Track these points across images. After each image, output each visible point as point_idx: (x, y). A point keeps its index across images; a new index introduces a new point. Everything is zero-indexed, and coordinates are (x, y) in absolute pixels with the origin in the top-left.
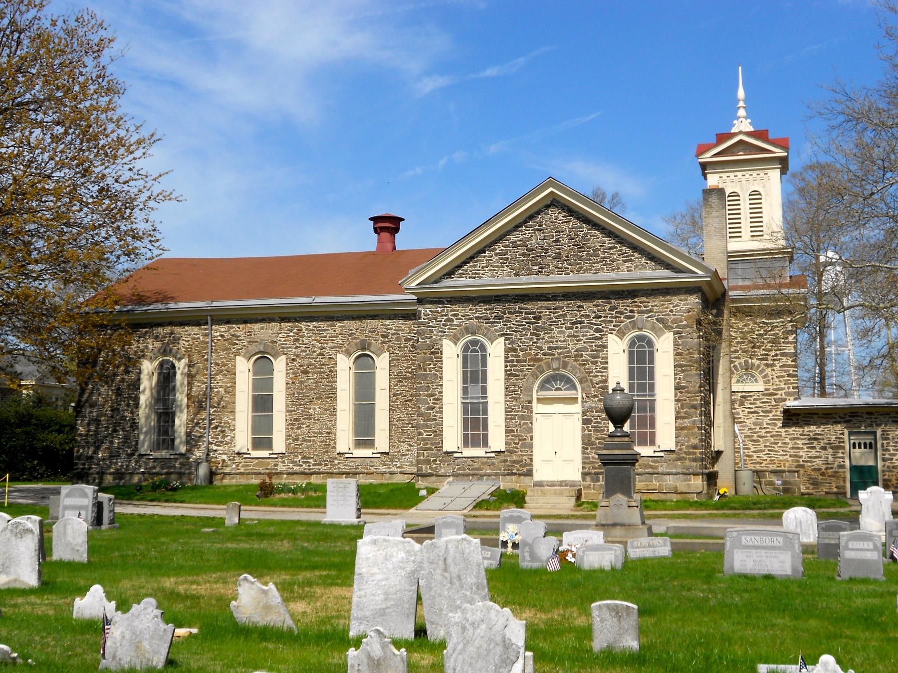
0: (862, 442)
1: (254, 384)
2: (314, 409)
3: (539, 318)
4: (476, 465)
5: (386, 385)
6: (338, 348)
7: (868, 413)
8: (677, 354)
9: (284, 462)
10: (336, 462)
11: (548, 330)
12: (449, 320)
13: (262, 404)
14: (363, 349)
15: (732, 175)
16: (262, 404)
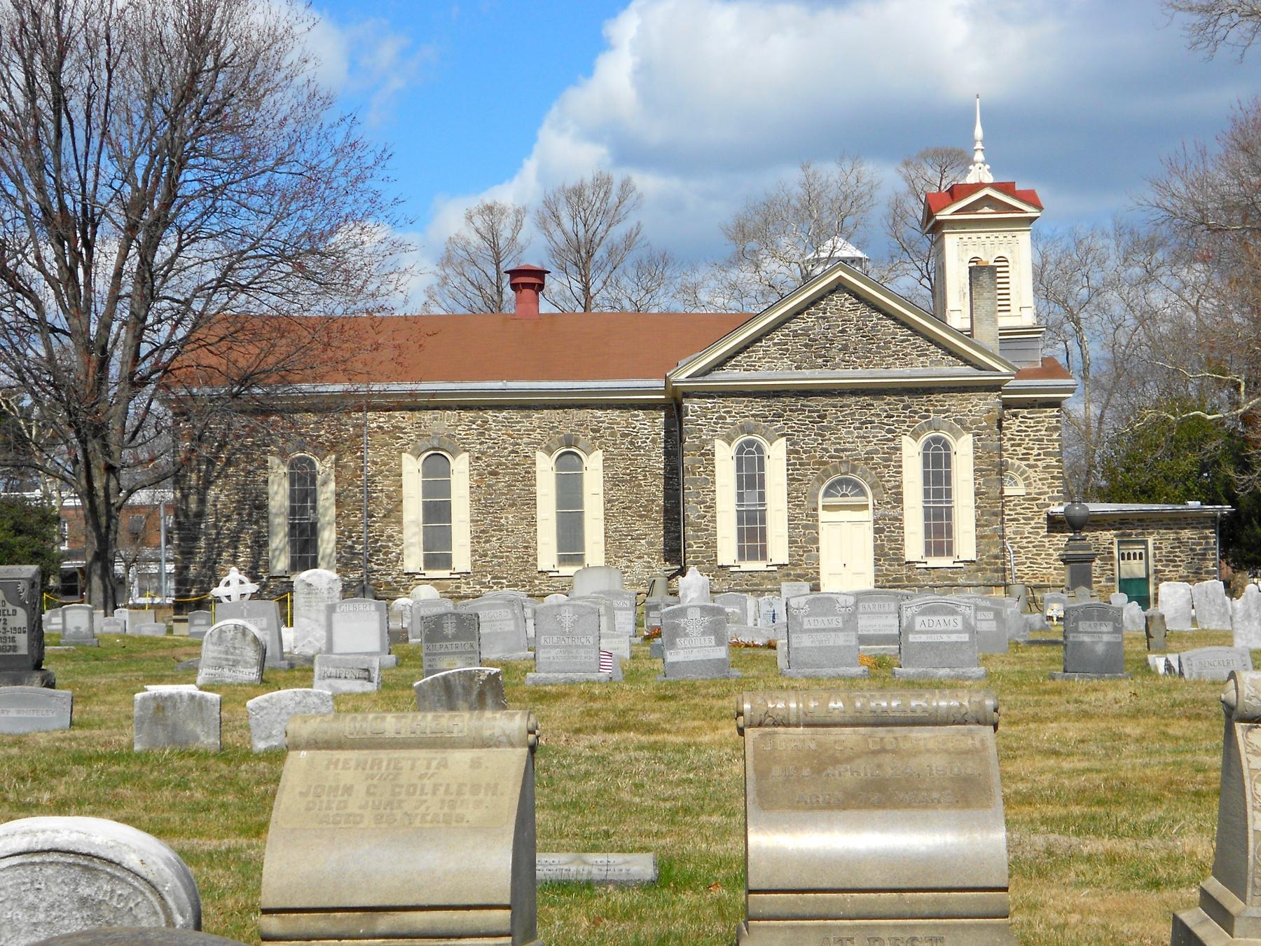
0: (1132, 552)
1: (424, 487)
2: (507, 518)
3: (824, 417)
4: (756, 581)
5: (600, 489)
6: (536, 444)
7: (1139, 520)
8: (976, 458)
9: (468, 583)
10: (537, 582)
11: (834, 430)
12: (721, 418)
13: (437, 512)
14: (569, 446)
15: (974, 236)
16: (437, 512)
